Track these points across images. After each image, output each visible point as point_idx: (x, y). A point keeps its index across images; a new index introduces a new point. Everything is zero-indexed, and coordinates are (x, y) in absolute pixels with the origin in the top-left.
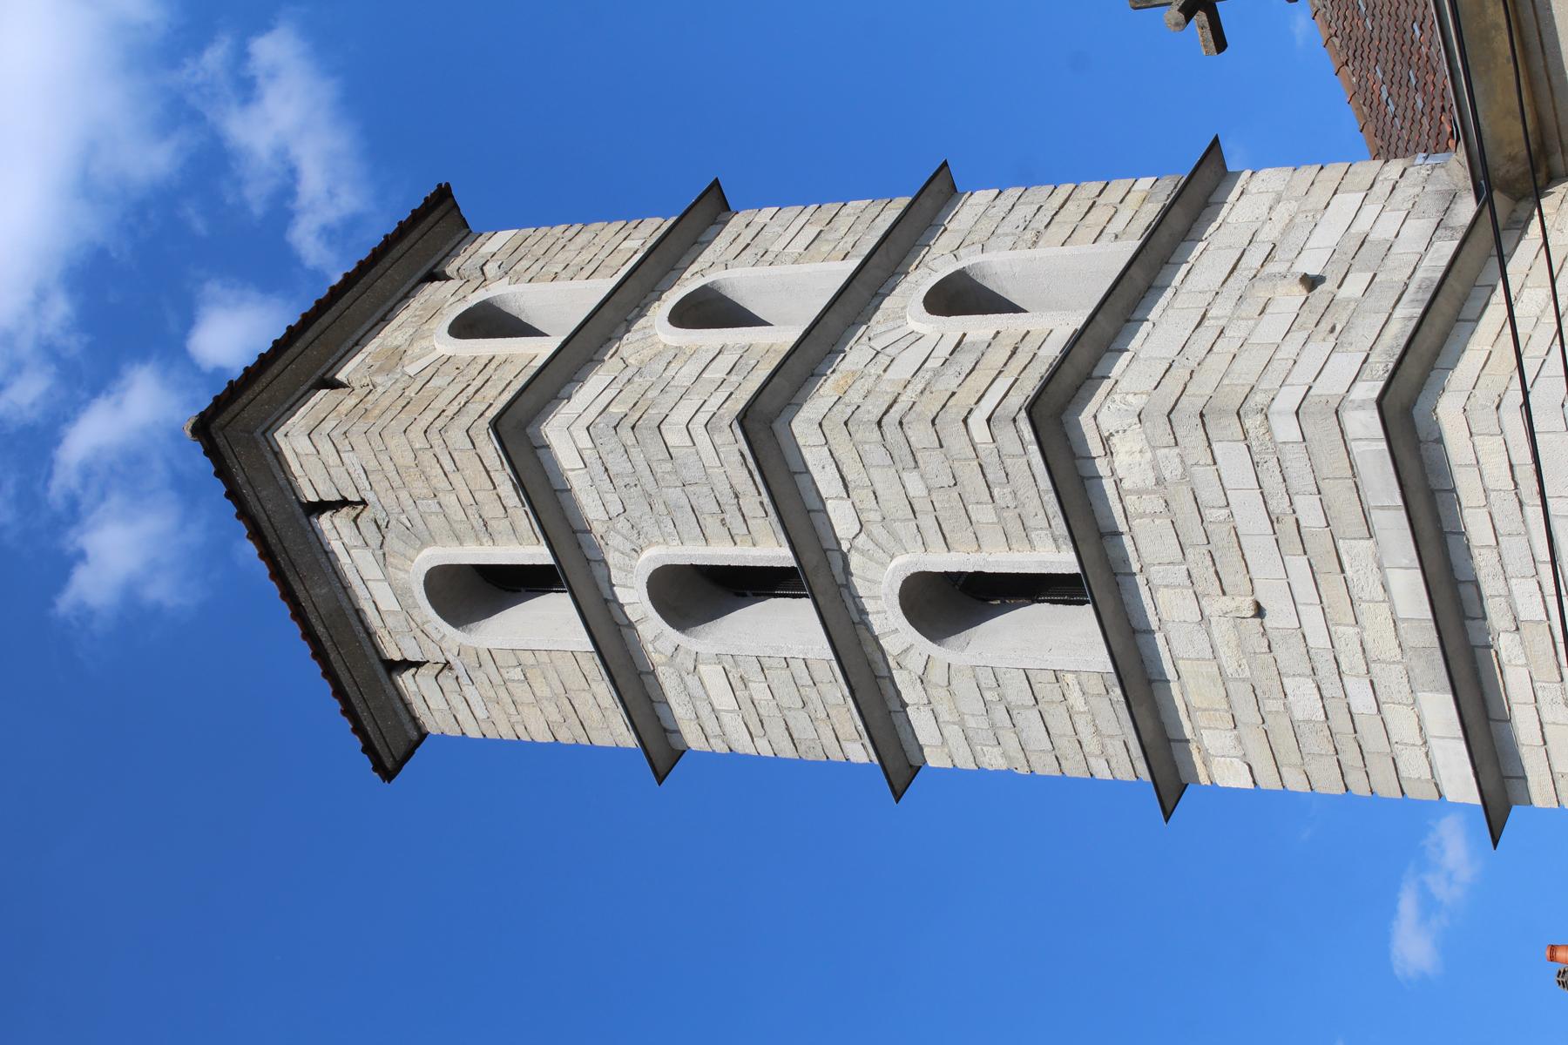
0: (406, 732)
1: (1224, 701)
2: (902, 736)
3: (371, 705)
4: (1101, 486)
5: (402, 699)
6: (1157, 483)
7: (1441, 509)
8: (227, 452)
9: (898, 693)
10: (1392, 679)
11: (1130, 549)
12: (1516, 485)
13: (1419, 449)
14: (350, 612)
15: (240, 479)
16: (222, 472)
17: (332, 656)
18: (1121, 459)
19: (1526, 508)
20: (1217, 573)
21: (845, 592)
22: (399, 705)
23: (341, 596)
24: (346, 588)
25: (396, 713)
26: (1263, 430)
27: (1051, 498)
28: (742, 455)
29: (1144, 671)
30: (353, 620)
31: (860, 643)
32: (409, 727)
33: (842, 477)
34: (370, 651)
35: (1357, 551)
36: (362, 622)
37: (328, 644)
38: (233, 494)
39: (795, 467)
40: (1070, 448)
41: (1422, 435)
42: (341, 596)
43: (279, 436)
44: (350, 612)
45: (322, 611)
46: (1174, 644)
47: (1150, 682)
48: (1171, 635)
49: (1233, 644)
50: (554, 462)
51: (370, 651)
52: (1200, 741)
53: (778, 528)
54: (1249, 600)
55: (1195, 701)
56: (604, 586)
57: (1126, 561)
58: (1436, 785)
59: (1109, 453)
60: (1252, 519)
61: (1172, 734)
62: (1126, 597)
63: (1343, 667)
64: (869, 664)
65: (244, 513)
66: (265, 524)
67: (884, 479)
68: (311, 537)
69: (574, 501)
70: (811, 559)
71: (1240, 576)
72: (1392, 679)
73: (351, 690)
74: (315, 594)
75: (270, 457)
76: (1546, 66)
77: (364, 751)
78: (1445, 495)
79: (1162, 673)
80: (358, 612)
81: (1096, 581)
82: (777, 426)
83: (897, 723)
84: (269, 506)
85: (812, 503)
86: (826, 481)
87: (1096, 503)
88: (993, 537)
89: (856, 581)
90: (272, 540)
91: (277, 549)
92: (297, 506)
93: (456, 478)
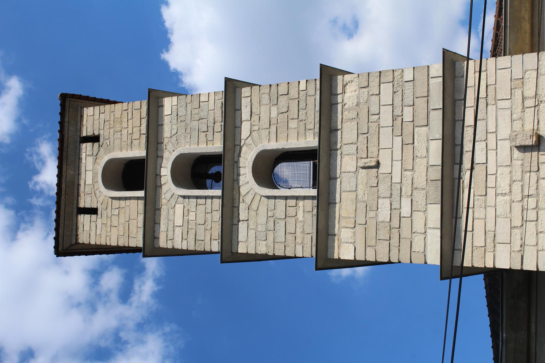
0: (72, 240)
1: (354, 213)
2: (234, 236)
3: (66, 223)
4: (337, 107)
5: (77, 226)
6: (357, 105)
7: (457, 108)
8: (67, 109)
9: (239, 214)
10: (419, 197)
11: (339, 137)
12: (487, 95)
13: (454, 80)
14: (76, 184)
15: (66, 120)
16: (62, 114)
17: (63, 197)
18: (347, 95)
19: (489, 107)
20: (367, 147)
21: (236, 164)
22: (75, 227)
23: (76, 177)
24: (79, 174)
25: (72, 230)
26: (400, 77)
27: (318, 115)
28: (222, 104)
29: (328, 198)
30: (76, 189)
31: (233, 189)
32: (74, 238)
33: (251, 111)
34: (75, 202)
35: (421, 132)
36: (78, 189)
37: (63, 192)
38: (61, 123)
39: (237, 108)
40: (331, 90)
41: (457, 74)
42: (76, 177)
43: (85, 109)
44: (76, 184)
45: (67, 179)
46: (343, 184)
47: (329, 204)
48: (343, 180)
49: (364, 183)
50: (162, 132)
51: (75, 202)
52: (339, 236)
53: (223, 137)
54: (375, 159)
55: (343, 214)
56: (158, 167)
57: (336, 143)
58: (425, 256)
59: (344, 92)
60: (386, 118)
61: (330, 232)
62: (332, 161)
63: (403, 193)
64: (233, 200)
65: (61, 131)
66: (66, 139)
67: (264, 109)
68: (78, 151)
69: (162, 129)
70: (228, 157)
71: (376, 147)
72: (419, 197)
73: (62, 213)
74: (69, 172)
75: (79, 116)
76: (537, 295)
77: (59, 122)
78: (459, 102)
79: (335, 199)
80: (79, 185)
81: (323, 155)
82: (237, 89)
83: (234, 230)
84: (70, 133)
85: (238, 124)
86: (245, 114)
87: (333, 116)
88: (293, 134)
89: (241, 159)
90: (65, 146)
91: (65, 149)
92: (78, 137)
93: (130, 122)
